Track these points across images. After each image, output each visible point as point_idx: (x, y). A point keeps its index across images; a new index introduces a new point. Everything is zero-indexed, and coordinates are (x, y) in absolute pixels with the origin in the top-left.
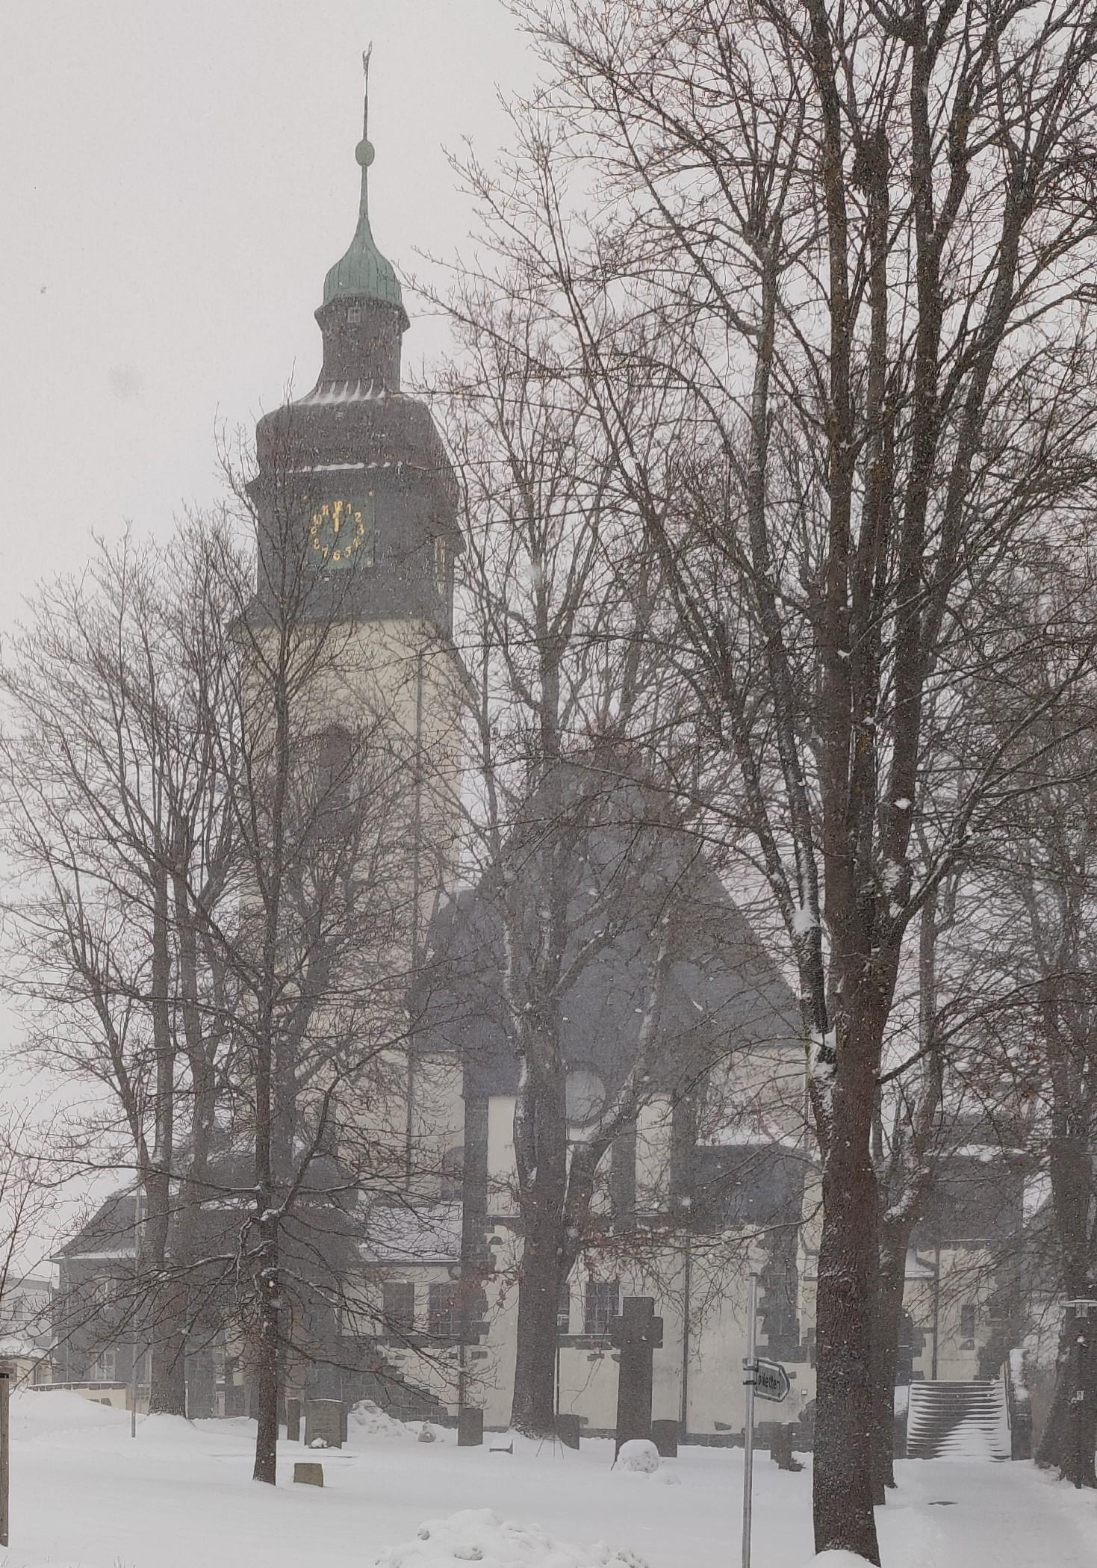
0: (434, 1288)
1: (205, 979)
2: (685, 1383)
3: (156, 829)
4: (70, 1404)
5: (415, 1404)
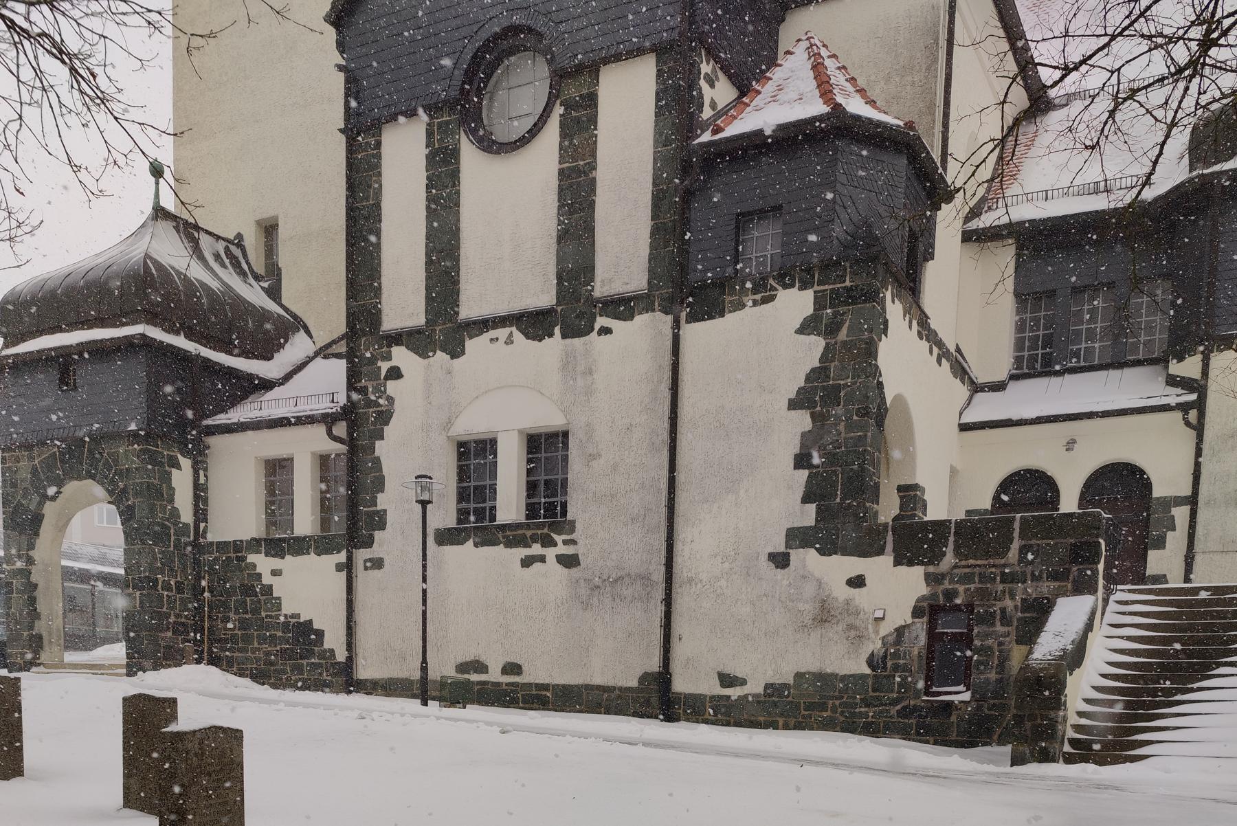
2: (668, 601)
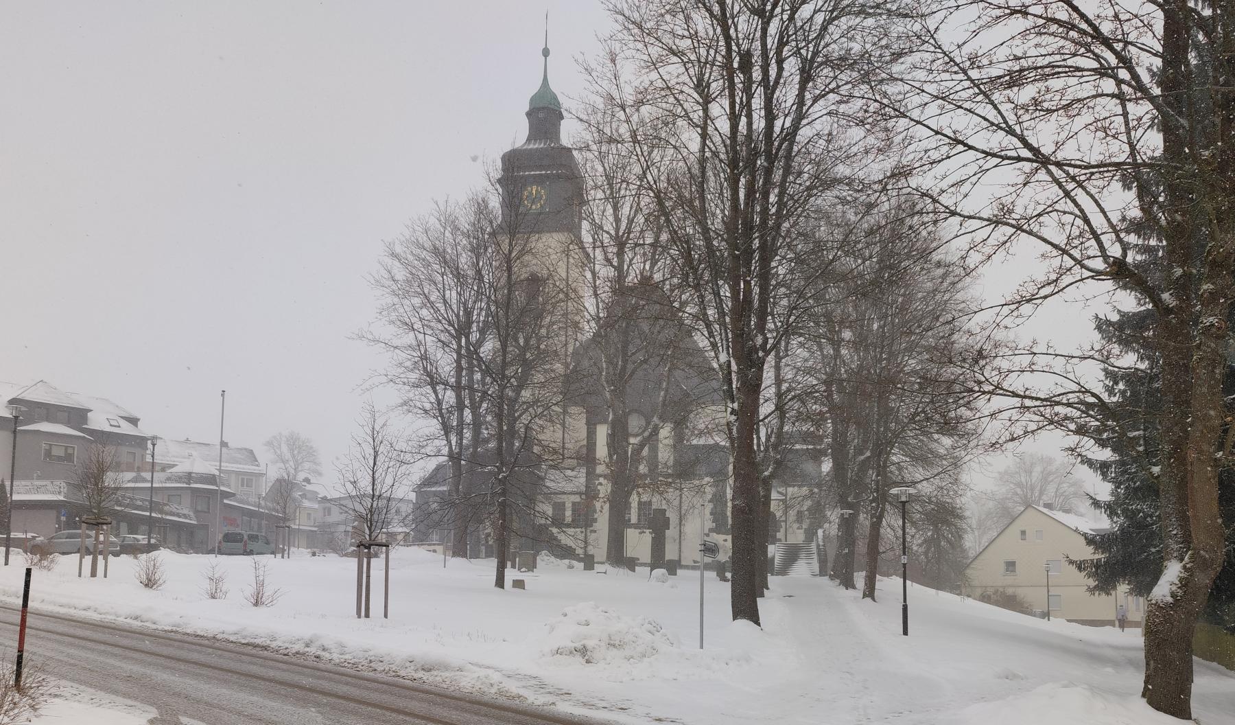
0: (574, 504)
1: (478, 376)
3: (458, 316)
4: (418, 553)
5: (565, 553)
